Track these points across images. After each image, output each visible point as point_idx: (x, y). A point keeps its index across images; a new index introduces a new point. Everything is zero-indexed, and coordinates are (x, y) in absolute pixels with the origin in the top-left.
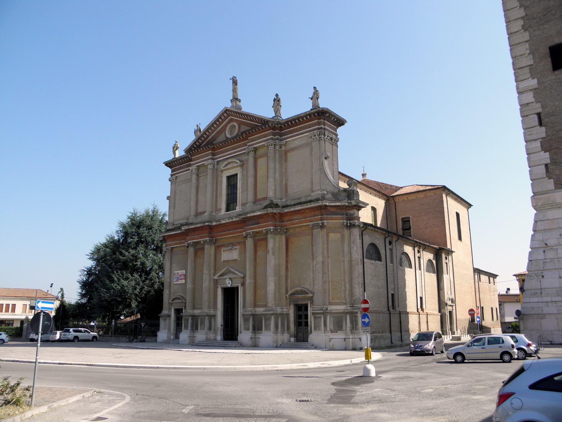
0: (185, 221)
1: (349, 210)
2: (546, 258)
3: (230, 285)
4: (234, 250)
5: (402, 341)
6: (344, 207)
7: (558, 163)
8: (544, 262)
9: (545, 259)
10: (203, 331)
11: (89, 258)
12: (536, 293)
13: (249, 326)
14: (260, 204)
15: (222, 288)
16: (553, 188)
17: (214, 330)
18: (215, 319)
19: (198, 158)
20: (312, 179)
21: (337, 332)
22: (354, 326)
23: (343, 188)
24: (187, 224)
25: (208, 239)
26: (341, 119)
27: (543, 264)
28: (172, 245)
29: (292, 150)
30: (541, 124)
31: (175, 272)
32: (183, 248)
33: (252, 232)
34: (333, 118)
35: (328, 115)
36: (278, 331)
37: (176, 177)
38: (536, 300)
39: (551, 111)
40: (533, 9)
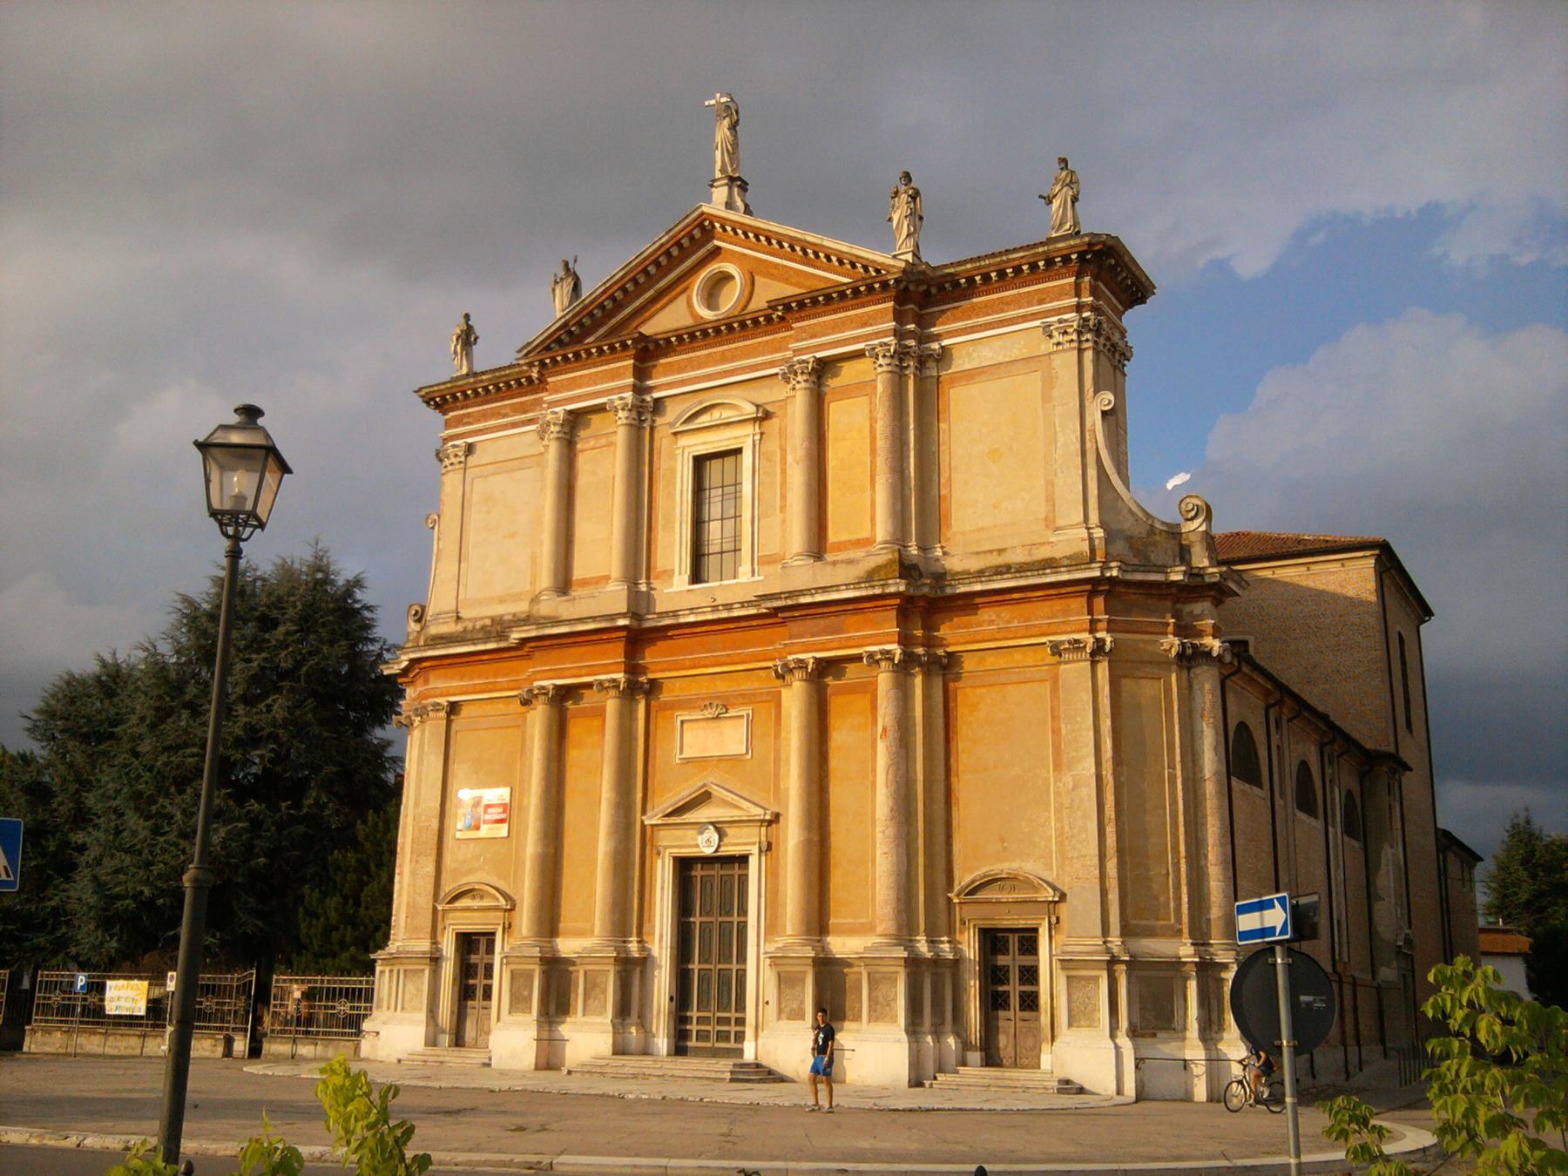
0: (522, 607)
1: (1184, 603)
4: (729, 722)
5: (1314, 1077)
6: (1174, 591)
11: (29, 730)
13: (802, 1002)
14: (850, 562)
15: (674, 858)
18: (643, 975)
19: (573, 384)
20: (1050, 484)
21: (1154, 1035)
23: (1163, 523)
24: (527, 620)
25: (622, 675)
32: (501, 707)
33: (815, 658)
34: (1124, 275)
35: (1113, 262)
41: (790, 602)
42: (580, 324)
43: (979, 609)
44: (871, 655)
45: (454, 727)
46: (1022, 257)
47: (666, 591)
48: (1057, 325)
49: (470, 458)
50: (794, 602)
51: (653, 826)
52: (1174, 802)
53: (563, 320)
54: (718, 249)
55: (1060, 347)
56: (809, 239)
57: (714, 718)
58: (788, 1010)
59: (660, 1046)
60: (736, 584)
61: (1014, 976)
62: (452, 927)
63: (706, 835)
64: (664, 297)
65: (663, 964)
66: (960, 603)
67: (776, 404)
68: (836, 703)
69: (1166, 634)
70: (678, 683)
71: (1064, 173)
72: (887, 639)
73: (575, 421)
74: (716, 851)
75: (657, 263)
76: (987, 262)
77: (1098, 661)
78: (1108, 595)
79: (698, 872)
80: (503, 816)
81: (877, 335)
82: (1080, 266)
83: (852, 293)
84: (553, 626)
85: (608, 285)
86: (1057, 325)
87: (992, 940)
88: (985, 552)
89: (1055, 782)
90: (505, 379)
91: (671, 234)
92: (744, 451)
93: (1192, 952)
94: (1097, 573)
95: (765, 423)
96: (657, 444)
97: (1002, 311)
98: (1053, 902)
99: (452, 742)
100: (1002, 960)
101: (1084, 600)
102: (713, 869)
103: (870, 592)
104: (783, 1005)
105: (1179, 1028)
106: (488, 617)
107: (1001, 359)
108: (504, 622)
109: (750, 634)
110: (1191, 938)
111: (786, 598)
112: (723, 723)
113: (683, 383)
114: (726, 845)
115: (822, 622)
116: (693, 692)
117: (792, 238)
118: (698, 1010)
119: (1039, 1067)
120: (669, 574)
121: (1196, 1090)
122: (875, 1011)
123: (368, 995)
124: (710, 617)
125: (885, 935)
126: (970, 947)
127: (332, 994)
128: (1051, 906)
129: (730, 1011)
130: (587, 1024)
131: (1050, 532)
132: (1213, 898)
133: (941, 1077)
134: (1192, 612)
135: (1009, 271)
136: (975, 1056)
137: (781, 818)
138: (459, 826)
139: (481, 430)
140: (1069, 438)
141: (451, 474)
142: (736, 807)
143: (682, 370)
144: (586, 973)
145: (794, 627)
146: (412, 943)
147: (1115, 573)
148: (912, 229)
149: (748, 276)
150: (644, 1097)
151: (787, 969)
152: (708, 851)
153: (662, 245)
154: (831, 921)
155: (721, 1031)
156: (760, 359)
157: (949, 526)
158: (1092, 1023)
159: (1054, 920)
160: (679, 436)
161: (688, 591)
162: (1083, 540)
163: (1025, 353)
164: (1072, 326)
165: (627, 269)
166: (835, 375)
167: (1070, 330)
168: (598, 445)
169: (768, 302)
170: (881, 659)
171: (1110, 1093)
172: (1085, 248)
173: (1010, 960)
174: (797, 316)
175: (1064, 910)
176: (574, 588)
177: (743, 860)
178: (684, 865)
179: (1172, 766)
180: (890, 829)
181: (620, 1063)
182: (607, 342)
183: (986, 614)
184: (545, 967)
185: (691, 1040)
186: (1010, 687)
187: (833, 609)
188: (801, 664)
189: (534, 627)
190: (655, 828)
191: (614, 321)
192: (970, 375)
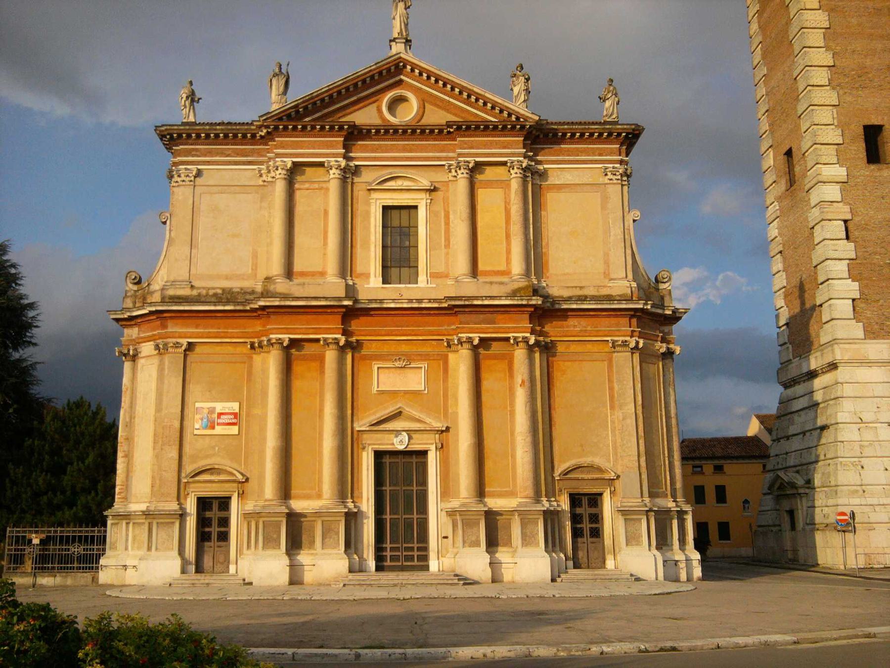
2: (863, 439)
6: (662, 319)
7: (869, 301)
8: (861, 446)
9: (861, 441)
12: (857, 491)
13: (478, 537)
16: (862, 336)
18: (356, 521)
27: (860, 448)
30: (848, 238)
31: (198, 405)
33: (479, 337)
37: (199, 171)
38: (857, 501)
39: (863, 222)
40: (844, 60)
41: (467, 303)
42: (306, 108)
43: (568, 318)
44: (325, 340)
45: (189, 359)
46: (596, 128)
47: (366, 286)
48: (184, 171)
49: (197, 179)
50: (470, 303)
51: (359, 431)
52: (662, 429)
53: (296, 103)
54: (401, 81)
55: (611, 182)
56: (475, 89)
57: (401, 367)
58: (470, 541)
59: (371, 565)
60: (417, 287)
61: (215, 523)
62: (193, 494)
63: (400, 438)
64: (361, 103)
65: (370, 516)
66: (559, 314)
67: (440, 183)
68: (485, 364)
69: (657, 341)
70: (374, 344)
71: (611, 88)
72: (524, 330)
73: (296, 169)
74: (406, 448)
75: (364, 81)
76: (577, 127)
77: (634, 353)
78: (639, 319)
79: (387, 460)
80: (234, 421)
81: (513, 155)
82: (623, 141)
83: (338, 128)
84: (293, 300)
85: (331, 87)
86: (611, 169)
87: (575, 500)
88: (572, 287)
89: (611, 416)
90: (234, 132)
91: (378, 65)
92: (419, 207)
93: (675, 505)
95: (433, 193)
96: (355, 193)
97: (578, 156)
99: (188, 369)
100: (208, 514)
101: (628, 319)
102: (398, 458)
103: (520, 303)
104: (466, 538)
105: (670, 544)
106: (239, 288)
107: (577, 182)
108: (233, 293)
109: (427, 319)
110: (672, 498)
111: (465, 300)
112: (407, 371)
113: (375, 159)
114: (413, 444)
115: (482, 316)
116: (385, 350)
117: (463, 87)
118: (390, 543)
119: (228, 572)
120: (367, 276)
121: (681, 575)
122: (526, 540)
123: (103, 540)
124: (405, 306)
125: (530, 498)
126: (564, 504)
127: (66, 540)
128: (610, 482)
129: (414, 543)
130: (325, 554)
131: (607, 280)
132: (677, 478)
133: (563, 576)
134: (664, 330)
135: (230, 135)
137: (450, 430)
138: (196, 425)
139: (208, 162)
140: (617, 231)
141: (182, 188)
142: (419, 421)
143: (391, 151)
144: (263, 522)
145: (461, 317)
146: (162, 504)
147: (649, 307)
148: (526, 98)
149: (422, 102)
150: (513, 596)
151: (467, 517)
152: (401, 447)
153: (370, 71)
154: (292, 492)
155: (407, 555)
156: (431, 154)
157: (548, 270)
158: (639, 543)
160: (372, 192)
161: (382, 288)
162: (627, 287)
163: (590, 181)
164: (618, 171)
165: (345, 80)
166: (481, 173)
167: (618, 173)
168: (312, 187)
169: (447, 122)
170: (275, 343)
171: (652, 579)
172: (631, 131)
173: (214, 514)
174: (462, 133)
175: (617, 483)
176: (294, 277)
177: (424, 453)
178: (379, 455)
179: (661, 410)
180: (529, 438)
181: (378, 578)
182: (320, 123)
183: (572, 322)
185: (386, 561)
186: (584, 363)
187: (492, 310)
188: (470, 340)
189: (278, 299)
190: (360, 433)
191: (326, 111)
192: (559, 188)
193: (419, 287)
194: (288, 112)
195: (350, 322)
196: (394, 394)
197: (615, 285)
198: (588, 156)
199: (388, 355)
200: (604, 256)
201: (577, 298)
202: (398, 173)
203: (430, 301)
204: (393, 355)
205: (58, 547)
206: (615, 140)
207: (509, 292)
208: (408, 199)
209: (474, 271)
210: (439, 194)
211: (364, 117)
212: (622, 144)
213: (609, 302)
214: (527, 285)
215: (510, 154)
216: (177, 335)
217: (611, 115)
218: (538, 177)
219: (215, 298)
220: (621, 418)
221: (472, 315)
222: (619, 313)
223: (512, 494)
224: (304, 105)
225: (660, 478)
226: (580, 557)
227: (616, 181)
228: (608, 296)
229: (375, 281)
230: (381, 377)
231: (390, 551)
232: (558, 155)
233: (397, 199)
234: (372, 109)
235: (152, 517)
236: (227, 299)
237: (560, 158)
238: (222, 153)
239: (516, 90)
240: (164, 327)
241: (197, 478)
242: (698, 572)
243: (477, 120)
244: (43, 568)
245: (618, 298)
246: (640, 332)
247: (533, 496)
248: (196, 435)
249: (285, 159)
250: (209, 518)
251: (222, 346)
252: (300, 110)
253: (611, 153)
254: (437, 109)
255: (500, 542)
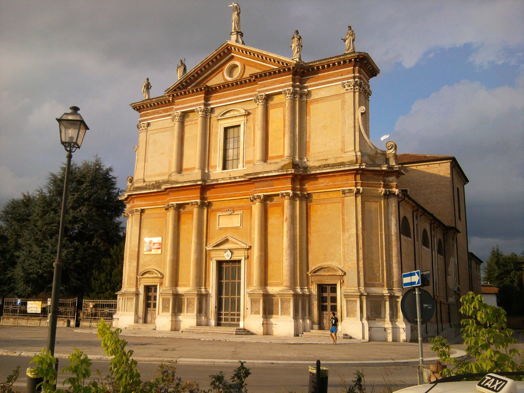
0: (166, 178)
3: (229, 258)
4: (235, 216)
6: (383, 173)
10: (191, 314)
13: (259, 309)
17: (205, 313)
19: (183, 103)
20: (343, 137)
21: (375, 320)
22: (395, 314)
26: (376, 68)
28: (143, 207)
29: (317, 100)
32: (158, 211)
33: (264, 195)
35: (366, 62)
36: (298, 316)
41: (255, 176)
42: (186, 82)
43: (318, 179)
45: (143, 217)
46: (335, 60)
49: (149, 128)
54: (233, 56)
55: (348, 91)
56: (264, 53)
57: (229, 215)
59: (212, 323)
60: (238, 170)
61: (329, 300)
63: (227, 253)
65: (213, 296)
67: (252, 110)
68: (270, 210)
70: (218, 203)
73: (184, 115)
75: (212, 61)
78: (361, 174)
79: (224, 265)
80: (159, 247)
81: (286, 86)
82: (355, 64)
84: (176, 184)
85: (196, 68)
86: (347, 83)
87: (322, 288)
88: (321, 160)
89: (342, 236)
91: (217, 51)
94: (358, 167)
95: (248, 116)
98: (341, 275)
100: (325, 295)
103: (282, 173)
104: (253, 309)
107: (328, 95)
108: (160, 183)
111: (254, 175)
112: (233, 216)
113: (221, 102)
114: (234, 256)
120: (215, 167)
121: (388, 338)
123: (115, 306)
124: (229, 181)
125: (287, 286)
126: (314, 290)
127: (103, 306)
132: (394, 274)
136: (316, 326)
137: (252, 248)
138: (144, 250)
143: (228, 96)
145: (257, 184)
146: (129, 289)
147: (364, 167)
148: (298, 50)
149: (243, 66)
151: (254, 297)
152: (228, 258)
154: (268, 282)
157: (309, 151)
158: (354, 316)
159: (342, 281)
162: (354, 156)
163: (336, 93)
165: (202, 63)
166: (272, 100)
168: (192, 123)
172: (357, 57)
173: (327, 295)
175: (345, 278)
178: (220, 263)
179: (381, 231)
182: (195, 88)
183: (321, 181)
184: (174, 297)
185: (222, 321)
187: (270, 179)
189: (170, 184)
190: (210, 251)
193: (239, 170)
194: (178, 86)
195: (206, 193)
196: (226, 229)
197: (346, 155)
198: (334, 78)
199: (224, 208)
200: (342, 138)
201: (324, 166)
202: (229, 109)
203: (240, 177)
204: (226, 208)
205: (100, 309)
206: (349, 65)
207: (279, 167)
208: (236, 122)
209: (265, 158)
210: (251, 116)
211: (215, 81)
212: (354, 66)
213: (338, 167)
214: (289, 162)
215: (284, 86)
216: (137, 206)
217: (349, 49)
218: (305, 97)
219: (152, 186)
220: (348, 237)
221: (261, 183)
222: (347, 173)
223: (280, 284)
224: (185, 80)
225: (378, 274)
226: (324, 323)
227: (350, 91)
228: (341, 163)
229: (219, 169)
230: (221, 220)
231: (224, 315)
232: (318, 81)
233: (230, 123)
234: (220, 75)
235: (125, 295)
236: (157, 186)
237: (317, 82)
238: (159, 113)
239: (293, 46)
240: (133, 202)
241: (145, 276)
242: (403, 336)
243: (268, 69)
244: (95, 319)
245: (348, 163)
246: (362, 183)
247: (289, 285)
248: (144, 255)
249: (178, 111)
250: (325, 297)
251: (155, 210)
252: (184, 84)
253: (348, 73)
254: (251, 68)
255: (274, 312)
